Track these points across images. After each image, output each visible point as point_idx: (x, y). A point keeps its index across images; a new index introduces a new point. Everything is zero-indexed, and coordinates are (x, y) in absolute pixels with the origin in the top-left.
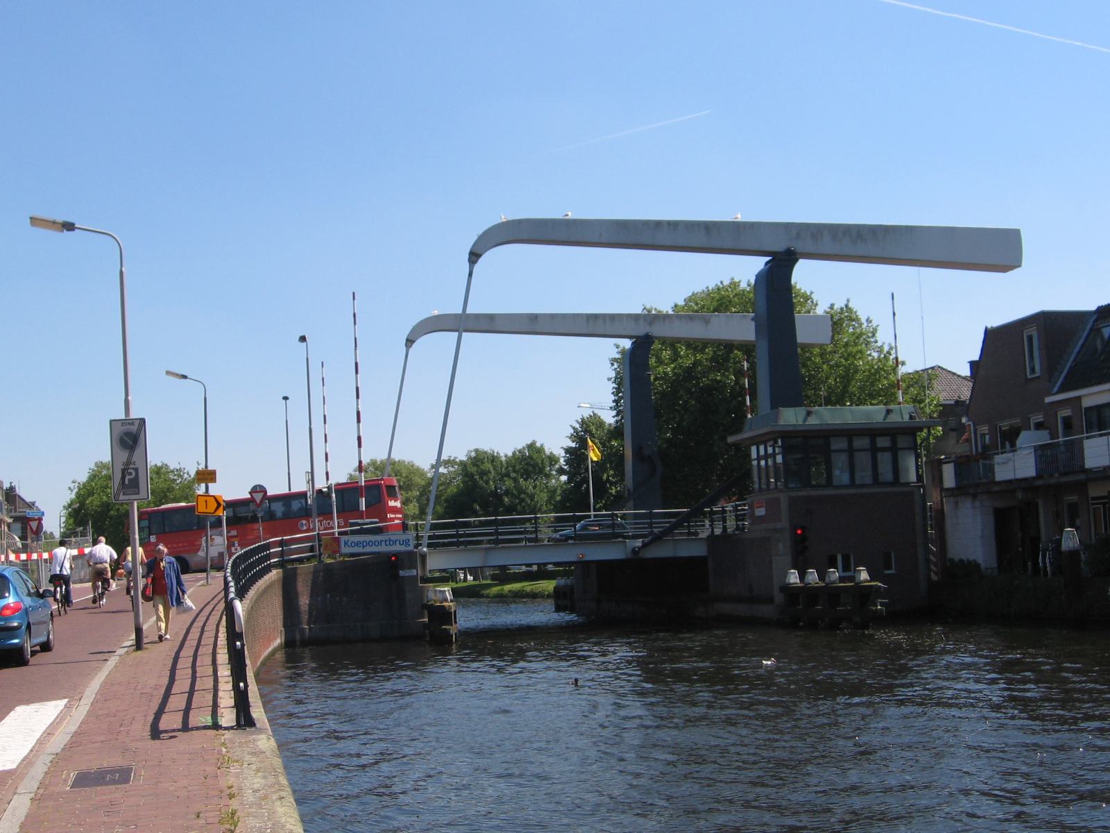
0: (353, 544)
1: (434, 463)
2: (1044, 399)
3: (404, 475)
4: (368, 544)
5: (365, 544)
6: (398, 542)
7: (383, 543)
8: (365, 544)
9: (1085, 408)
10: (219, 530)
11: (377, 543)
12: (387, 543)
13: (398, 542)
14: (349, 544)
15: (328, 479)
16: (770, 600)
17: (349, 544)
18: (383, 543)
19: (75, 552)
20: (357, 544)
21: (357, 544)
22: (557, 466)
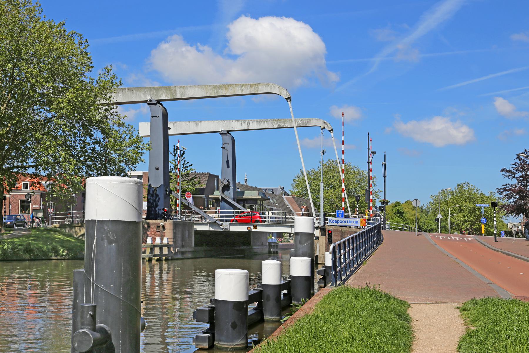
0: (333, 221)
1: (226, 191)
2: (43, 215)
3: (284, 256)
4: (340, 222)
5: (338, 222)
6: (353, 222)
7: (346, 222)
8: (338, 222)
9: (88, 221)
10: (306, 211)
11: (344, 222)
12: (348, 222)
13: (353, 222)
14: (331, 221)
15: (149, 182)
16: (77, 235)
17: (331, 221)
18: (346, 222)
19: (283, 195)
20: (335, 221)
21: (335, 221)
22: (51, 250)
